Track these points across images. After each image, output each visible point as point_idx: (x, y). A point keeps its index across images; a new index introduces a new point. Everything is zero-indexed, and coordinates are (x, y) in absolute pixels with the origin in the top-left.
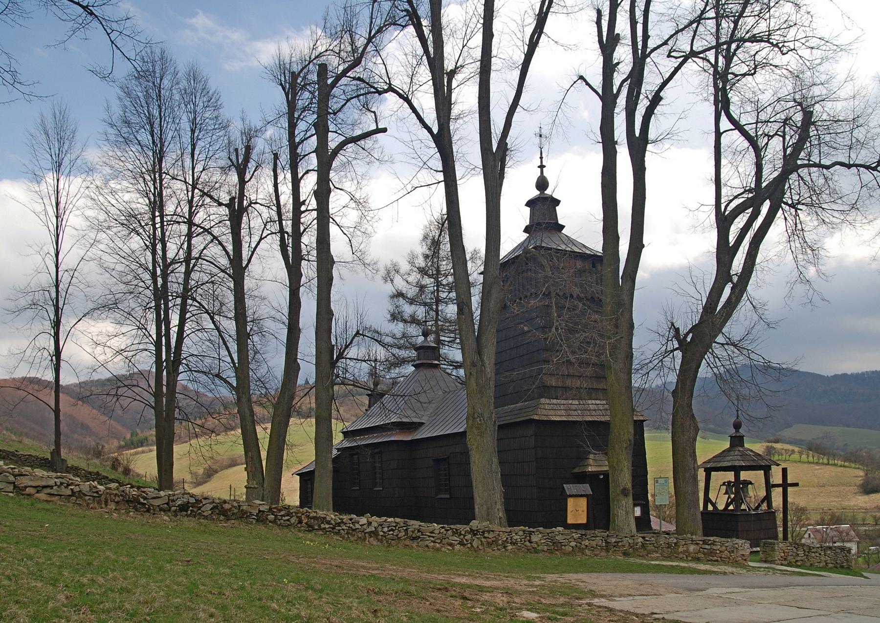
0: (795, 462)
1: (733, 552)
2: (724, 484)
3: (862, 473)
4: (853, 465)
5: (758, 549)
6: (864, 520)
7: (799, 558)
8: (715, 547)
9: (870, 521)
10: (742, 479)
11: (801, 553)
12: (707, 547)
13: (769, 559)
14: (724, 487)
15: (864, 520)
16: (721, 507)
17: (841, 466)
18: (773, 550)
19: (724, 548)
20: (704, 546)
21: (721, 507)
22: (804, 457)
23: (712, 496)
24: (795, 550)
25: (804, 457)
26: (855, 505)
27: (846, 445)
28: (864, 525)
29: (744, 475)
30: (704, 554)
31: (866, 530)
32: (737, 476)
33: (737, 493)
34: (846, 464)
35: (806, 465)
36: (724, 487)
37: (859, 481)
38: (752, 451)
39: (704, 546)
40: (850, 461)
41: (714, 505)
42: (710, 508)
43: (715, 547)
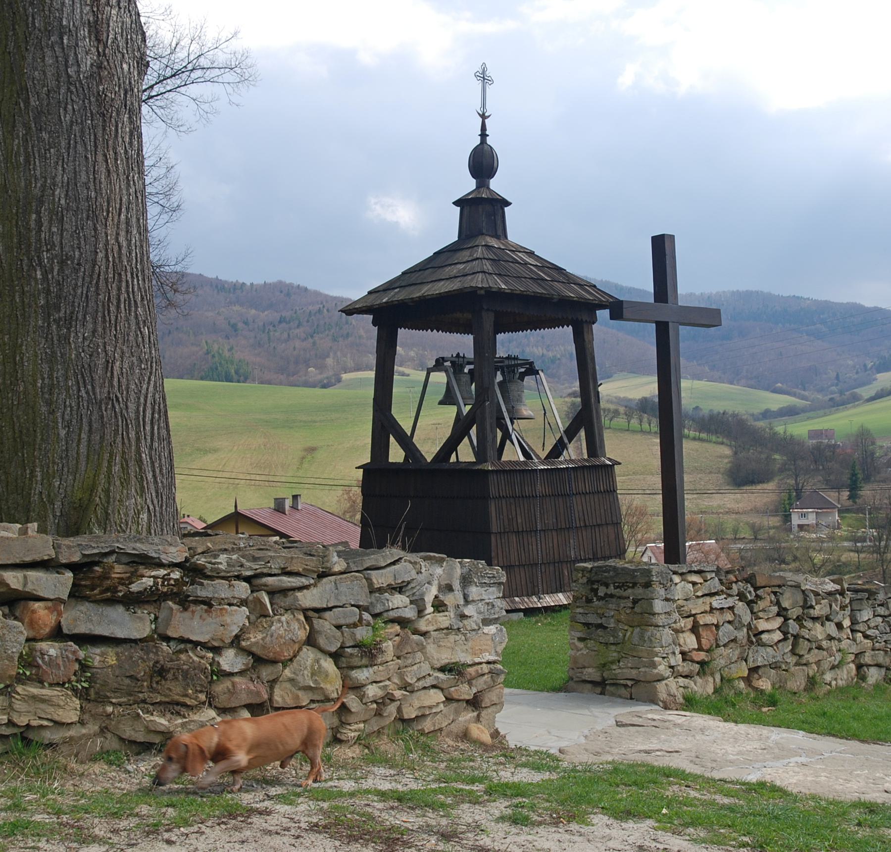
0: (621, 430)
1: (370, 652)
3: (727, 451)
4: (714, 438)
5: (562, 599)
6: (736, 531)
7: (761, 656)
8: (193, 625)
9: (746, 533)
10: (501, 353)
11: (769, 625)
12: (133, 625)
13: (623, 671)
14: (440, 378)
15: (736, 531)
16: (429, 451)
17: (694, 439)
18: (643, 617)
19: (287, 628)
20: (84, 618)
21: (429, 451)
22: (634, 422)
24: (741, 607)
25: (634, 422)
26: (719, 506)
27: (697, 407)
28: (736, 540)
29: (508, 344)
30: (91, 693)
31: (740, 550)
32: (485, 347)
33: (483, 394)
34: (703, 435)
35: (638, 436)
36: (440, 378)
37: (725, 464)
38: (531, 254)
39: (84, 618)
40: (709, 431)
41: (406, 442)
42: (396, 454)
43: (193, 625)
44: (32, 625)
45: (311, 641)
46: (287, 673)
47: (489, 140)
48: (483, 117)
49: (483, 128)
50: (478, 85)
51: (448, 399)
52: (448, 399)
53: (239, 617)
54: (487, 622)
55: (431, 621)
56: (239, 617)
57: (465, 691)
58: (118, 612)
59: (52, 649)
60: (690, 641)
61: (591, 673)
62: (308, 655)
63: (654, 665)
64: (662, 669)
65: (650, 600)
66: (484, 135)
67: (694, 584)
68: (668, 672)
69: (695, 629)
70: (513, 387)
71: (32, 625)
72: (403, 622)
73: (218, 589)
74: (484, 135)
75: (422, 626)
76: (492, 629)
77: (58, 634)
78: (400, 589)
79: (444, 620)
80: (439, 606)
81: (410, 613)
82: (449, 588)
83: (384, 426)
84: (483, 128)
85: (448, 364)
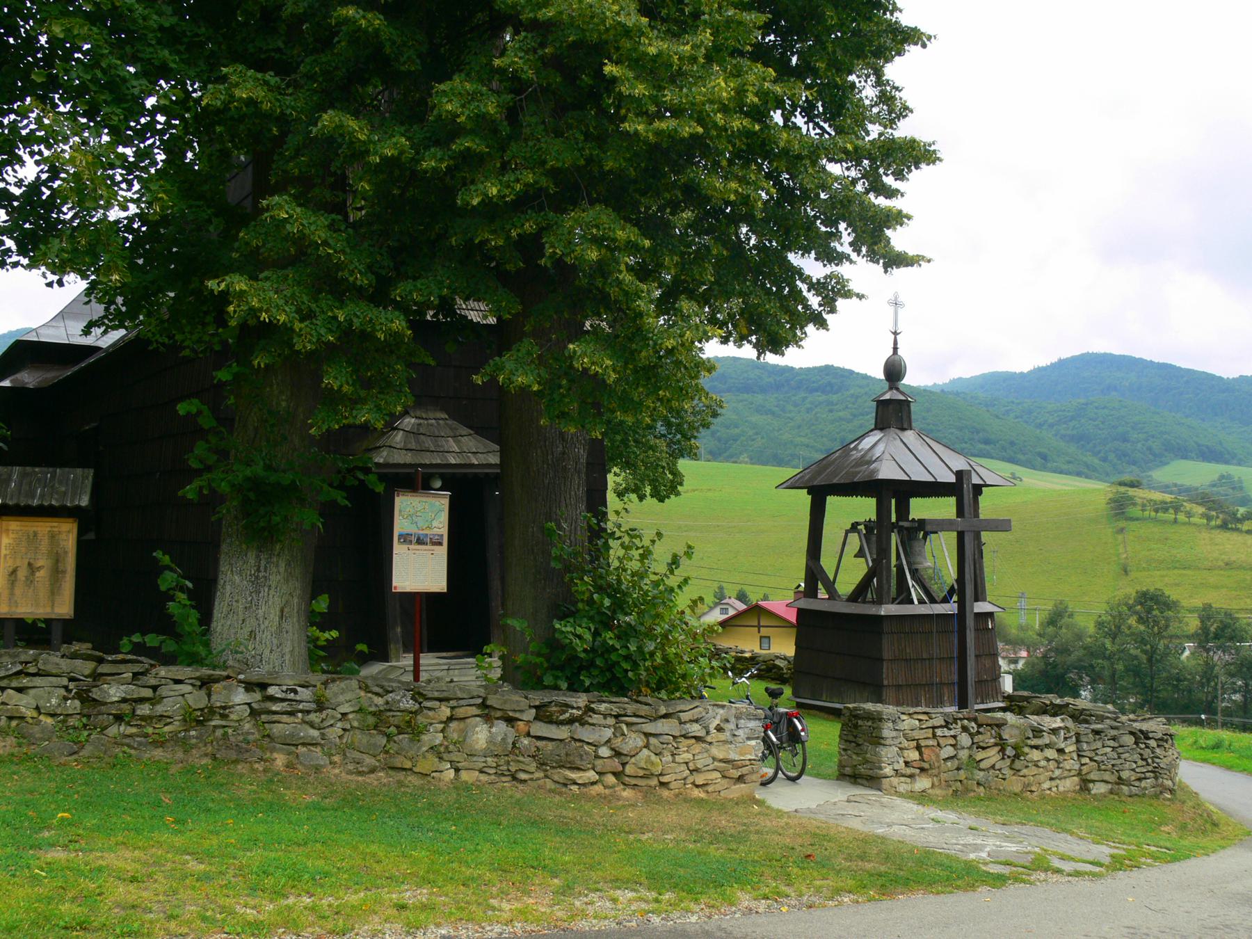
2: (854, 527)
8: (585, 733)
12: (562, 733)
18: (878, 741)
20: (540, 729)
23: (827, 562)
44: (517, 731)
45: (647, 746)
46: (633, 760)
47: (900, 352)
48: (895, 333)
49: (895, 343)
50: (892, 309)
51: (860, 554)
52: (860, 554)
53: (608, 733)
54: (748, 739)
55: (714, 736)
56: (608, 733)
57: (736, 773)
58: (553, 727)
59: (526, 741)
60: (914, 755)
61: (848, 770)
62: (645, 751)
63: (881, 768)
64: (888, 770)
65: (880, 729)
66: (895, 349)
67: (920, 720)
68: (893, 773)
69: (918, 748)
70: (917, 546)
71: (517, 731)
72: (698, 739)
73: (596, 719)
74: (895, 349)
75: (709, 739)
76: (753, 743)
77: (528, 735)
78: (696, 721)
79: (722, 736)
80: (719, 729)
81: (702, 733)
82: (727, 721)
83: (814, 575)
84: (895, 343)
85: (862, 527)
